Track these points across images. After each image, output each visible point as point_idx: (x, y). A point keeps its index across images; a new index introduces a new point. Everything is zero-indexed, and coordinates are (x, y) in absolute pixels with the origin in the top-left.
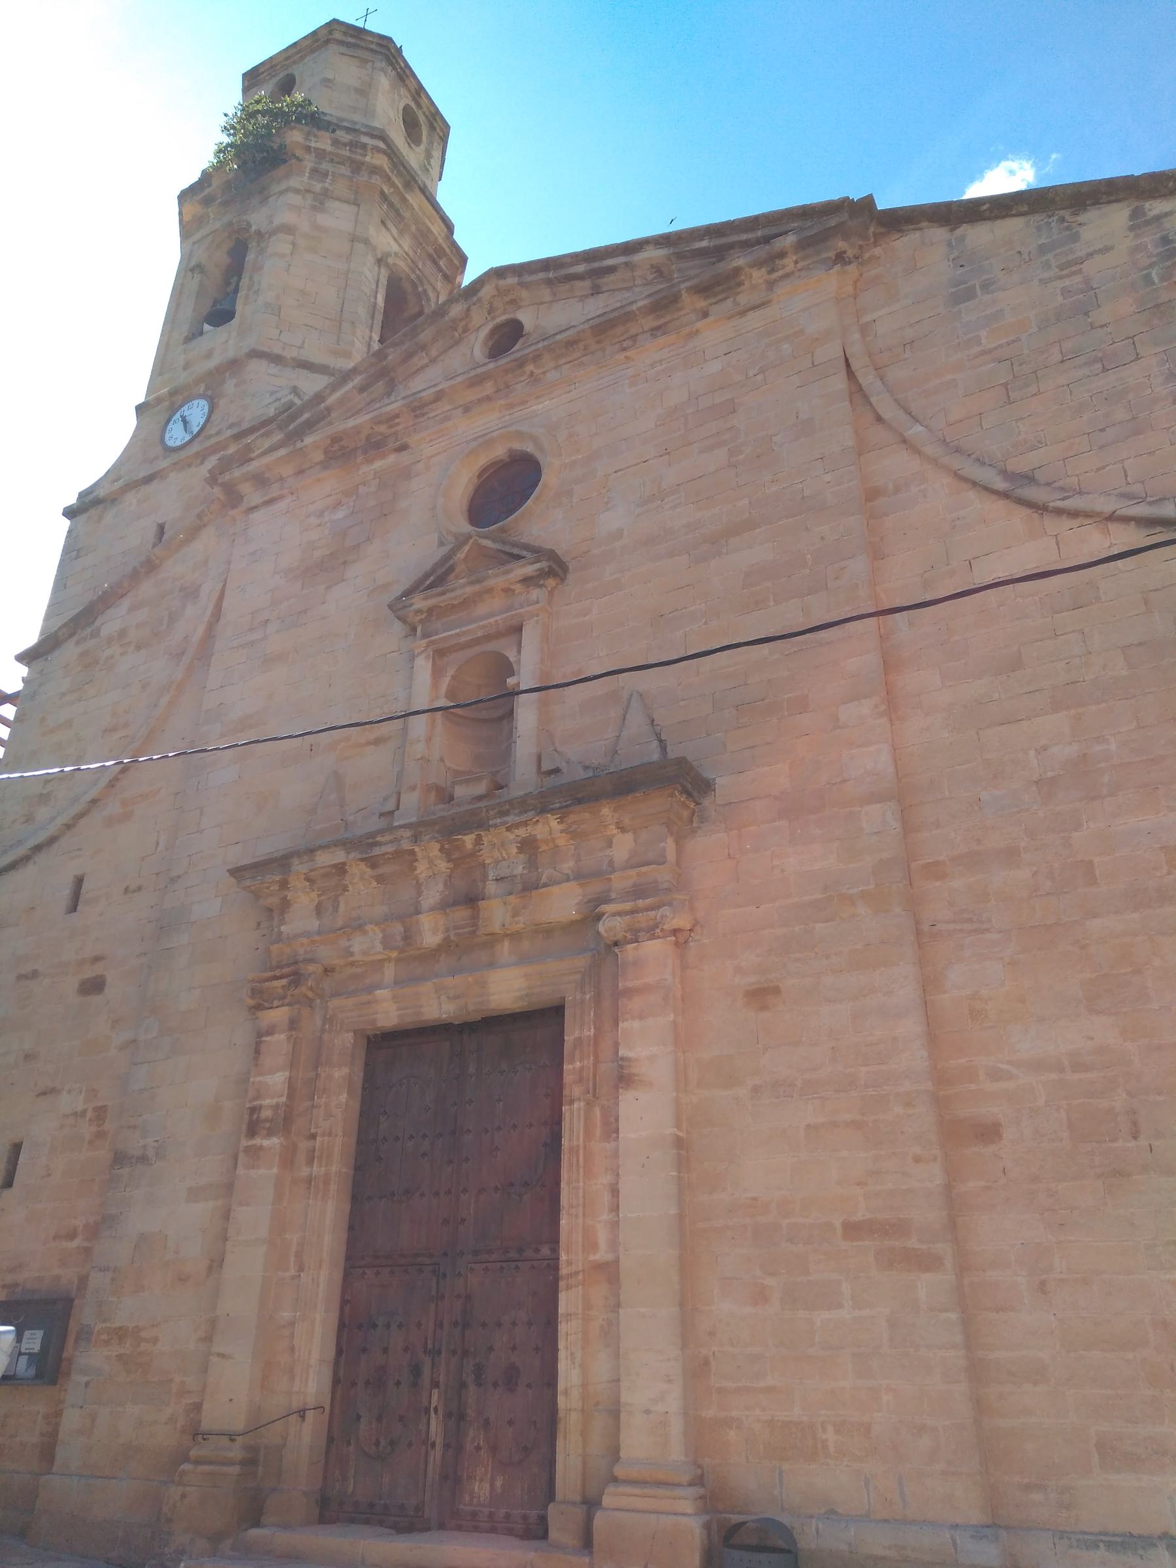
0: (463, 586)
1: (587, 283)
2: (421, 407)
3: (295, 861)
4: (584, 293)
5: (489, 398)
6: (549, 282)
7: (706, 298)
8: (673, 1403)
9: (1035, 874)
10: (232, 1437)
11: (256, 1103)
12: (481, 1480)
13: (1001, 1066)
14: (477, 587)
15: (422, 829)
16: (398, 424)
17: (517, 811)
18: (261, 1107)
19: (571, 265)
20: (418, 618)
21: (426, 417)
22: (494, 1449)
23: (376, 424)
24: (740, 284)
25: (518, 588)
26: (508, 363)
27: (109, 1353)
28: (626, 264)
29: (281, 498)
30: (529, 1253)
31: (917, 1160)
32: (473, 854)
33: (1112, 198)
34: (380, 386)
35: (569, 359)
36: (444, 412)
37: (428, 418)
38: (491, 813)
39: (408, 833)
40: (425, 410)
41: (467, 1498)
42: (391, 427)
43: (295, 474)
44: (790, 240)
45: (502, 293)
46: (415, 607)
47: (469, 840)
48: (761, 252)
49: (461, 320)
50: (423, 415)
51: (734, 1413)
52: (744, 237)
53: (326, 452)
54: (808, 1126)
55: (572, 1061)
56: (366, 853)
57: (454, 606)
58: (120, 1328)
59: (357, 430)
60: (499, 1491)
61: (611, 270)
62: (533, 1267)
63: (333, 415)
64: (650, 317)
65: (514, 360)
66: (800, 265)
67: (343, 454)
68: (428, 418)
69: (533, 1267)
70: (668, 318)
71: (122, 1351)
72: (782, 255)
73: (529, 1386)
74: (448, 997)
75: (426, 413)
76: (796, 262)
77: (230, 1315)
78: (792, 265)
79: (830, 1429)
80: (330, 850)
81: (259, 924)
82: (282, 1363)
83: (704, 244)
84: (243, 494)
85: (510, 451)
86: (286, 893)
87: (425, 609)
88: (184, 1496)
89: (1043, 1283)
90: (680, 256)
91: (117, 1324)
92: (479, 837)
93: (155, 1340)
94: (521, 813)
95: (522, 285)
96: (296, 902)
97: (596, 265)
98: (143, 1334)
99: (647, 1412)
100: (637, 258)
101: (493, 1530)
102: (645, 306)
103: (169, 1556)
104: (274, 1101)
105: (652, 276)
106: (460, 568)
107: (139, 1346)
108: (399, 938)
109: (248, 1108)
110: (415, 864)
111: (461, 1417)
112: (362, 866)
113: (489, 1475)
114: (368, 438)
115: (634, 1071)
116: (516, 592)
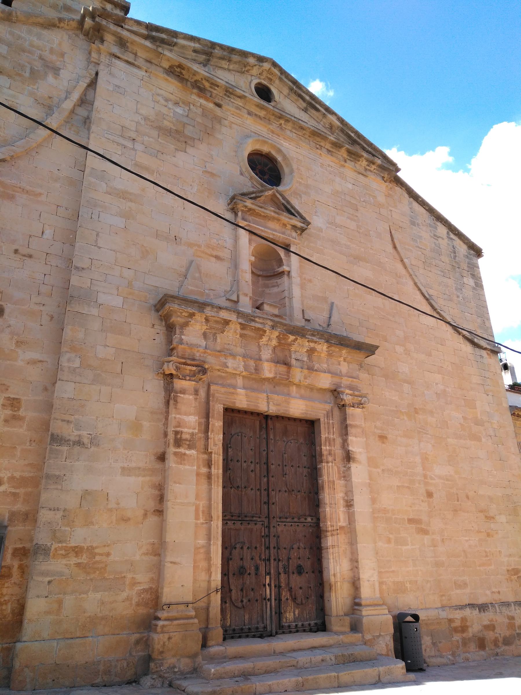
0: (271, 211)
1: (304, 105)
2: (231, 93)
3: (209, 308)
4: (300, 106)
5: (260, 117)
6: (291, 89)
7: (348, 155)
8: (375, 578)
9: (437, 421)
10: (187, 604)
11: (178, 429)
12: (290, 612)
13: (432, 475)
14: (276, 216)
15: (279, 325)
16: (215, 89)
17: (318, 337)
18: (182, 432)
19: (304, 92)
20: (243, 209)
21: (229, 99)
22: (294, 599)
23: (205, 79)
24: (359, 161)
25: (289, 227)
26: (277, 112)
27: (68, 562)
28: (324, 114)
29: (139, 68)
30: (302, 520)
31: (423, 501)
32: (290, 345)
33: (444, 224)
34: (202, 58)
35: (296, 132)
36: (238, 104)
37: (230, 100)
38: (309, 333)
39: (270, 323)
40: (232, 96)
41: (284, 620)
42: (211, 87)
43: (145, 59)
44: (379, 162)
45: (269, 71)
46: (247, 204)
47: (292, 338)
48: (370, 157)
49: (250, 66)
50: (229, 97)
51: (384, 580)
52: (365, 146)
53: (171, 67)
54: (397, 486)
55: (326, 445)
56: (248, 322)
57: (260, 215)
58: (77, 547)
59: (195, 73)
60: (297, 616)
61: (317, 110)
62: (304, 526)
63: (175, 48)
64: (330, 145)
65: (281, 114)
66: (375, 171)
67: (179, 76)
68: (230, 100)
69: (304, 526)
70: (334, 150)
71: (79, 561)
72: (374, 163)
73: (307, 573)
74: (274, 404)
75: (231, 97)
76: (374, 169)
77: (176, 541)
78: (373, 169)
79: (408, 583)
80: (230, 313)
81: (153, 325)
82: (201, 566)
83: (352, 135)
84: (105, 39)
85: (270, 152)
86: (190, 320)
87: (249, 207)
88: (169, 638)
89: (443, 539)
90: (342, 131)
91: (73, 544)
92: (296, 339)
93: (108, 554)
94: (319, 338)
95: (280, 79)
96: (191, 326)
97: (313, 103)
98: (97, 551)
99: (369, 581)
100: (330, 116)
101: (297, 631)
102: (333, 140)
103: (165, 671)
104: (191, 431)
105: (328, 126)
106: (262, 198)
107: (94, 558)
108: (253, 368)
109: (173, 431)
110: (263, 337)
111: (280, 587)
112: (238, 326)
113: (293, 609)
114: (196, 81)
115: (355, 457)
116: (287, 228)
